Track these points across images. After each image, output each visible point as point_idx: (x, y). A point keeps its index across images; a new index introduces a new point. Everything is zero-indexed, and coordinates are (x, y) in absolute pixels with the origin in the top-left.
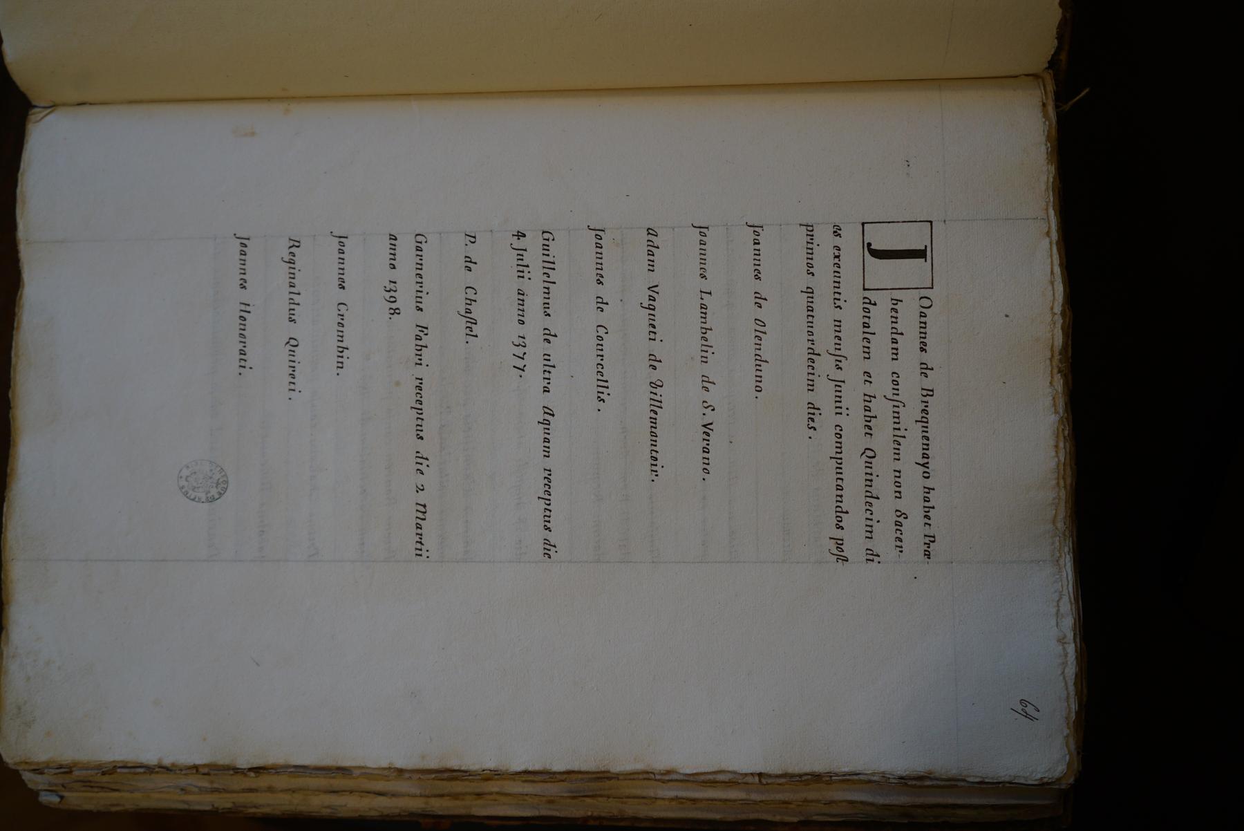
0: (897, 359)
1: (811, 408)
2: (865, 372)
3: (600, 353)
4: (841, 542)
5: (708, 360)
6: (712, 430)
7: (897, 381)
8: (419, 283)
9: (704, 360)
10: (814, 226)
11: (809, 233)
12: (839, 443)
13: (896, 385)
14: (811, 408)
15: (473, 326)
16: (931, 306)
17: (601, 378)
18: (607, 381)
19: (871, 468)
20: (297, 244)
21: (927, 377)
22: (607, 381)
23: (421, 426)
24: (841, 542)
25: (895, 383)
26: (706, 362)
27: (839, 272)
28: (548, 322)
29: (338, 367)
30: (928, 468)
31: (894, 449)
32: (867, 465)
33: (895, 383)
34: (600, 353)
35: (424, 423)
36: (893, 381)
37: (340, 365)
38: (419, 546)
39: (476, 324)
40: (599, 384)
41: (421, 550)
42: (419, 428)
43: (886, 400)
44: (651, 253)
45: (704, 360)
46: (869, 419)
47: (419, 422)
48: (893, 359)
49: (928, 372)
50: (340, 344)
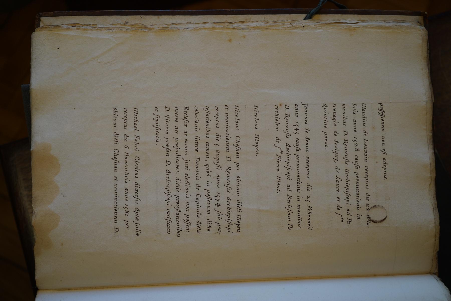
2: (186, 174)
3: (186, 165)
5: (228, 128)
8: (197, 147)
9: (299, 200)
15: (209, 114)
16: (230, 161)
23: (368, 184)
26: (300, 201)
29: (365, 161)
31: (207, 155)
34: (186, 165)
35: (368, 183)
37: (366, 160)
39: (210, 113)
42: (367, 185)
43: (153, 115)
45: (299, 200)
46: (115, 112)
47: (367, 183)
49: (279, 141)
50: (126, 172)
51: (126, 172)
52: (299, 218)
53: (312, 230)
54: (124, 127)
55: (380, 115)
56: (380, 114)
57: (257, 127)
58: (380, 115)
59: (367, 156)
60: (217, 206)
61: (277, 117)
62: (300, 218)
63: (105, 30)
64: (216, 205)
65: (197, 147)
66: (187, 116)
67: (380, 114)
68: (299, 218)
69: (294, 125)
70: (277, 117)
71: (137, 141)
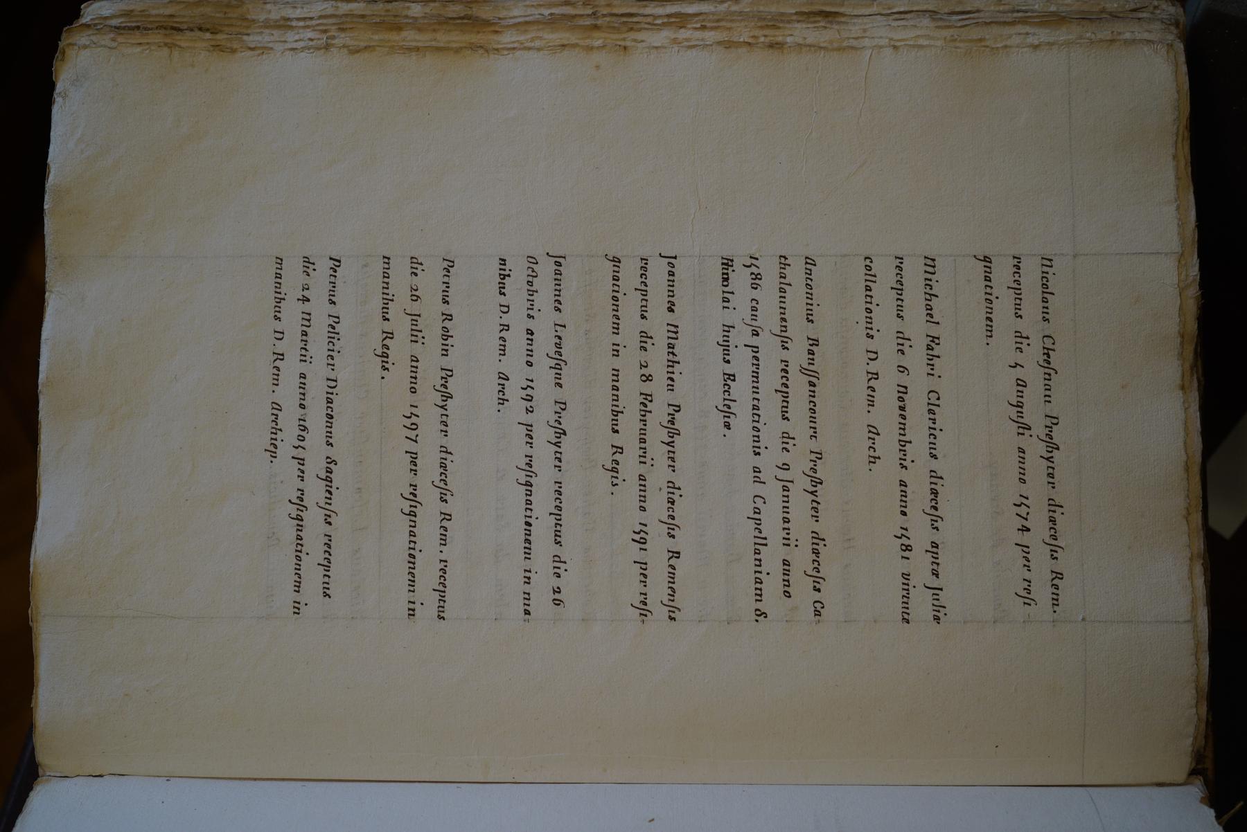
0: (761, 601)
1: (1018, 337)
4: (415, 456)
6: (733, 293)
7: (870, 267)
8: (331, 365)
10: (823, 454)
11: (901, 448)
12: (330, 422)
13: (869, 313)
14: (1018, 337)
17: (759, 535)
18: (765, 539)
19: (815, 422)
20: (448, 517)
21: (1022, 352)
22: (765, 539)
24: (415, 456)
25: (754, 309)
27: (935, 444)
28: (934, 465)
30: (560, 447)
32: (811, 419)
33: (754, 309)
36: (866, 266)
38: (303, 352)
40: (757, 542)
41: (305, 356)
44: (758, 470)
48: (756, 600)
50: (902, 438)
51: (902, 438)
52: (385, 296)
53: (393, 295)
54: (806, 317)
55: (806, 372)
56: (803, 371)
57: (1020, 313)
58: (806, 372)
59: (526, 288)
60: (302, 302)
61: (274, 436)
62: (388, 294)
63: (880, 44)
64: (298, 300)
65: (331, 365)
66: (786, 284)
67: (803, 371)
68: (385, 296)
69: (744, 265)
70: (274, 436)
71: (932, 349)
